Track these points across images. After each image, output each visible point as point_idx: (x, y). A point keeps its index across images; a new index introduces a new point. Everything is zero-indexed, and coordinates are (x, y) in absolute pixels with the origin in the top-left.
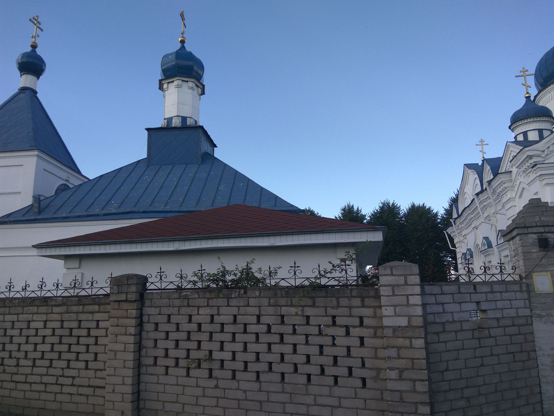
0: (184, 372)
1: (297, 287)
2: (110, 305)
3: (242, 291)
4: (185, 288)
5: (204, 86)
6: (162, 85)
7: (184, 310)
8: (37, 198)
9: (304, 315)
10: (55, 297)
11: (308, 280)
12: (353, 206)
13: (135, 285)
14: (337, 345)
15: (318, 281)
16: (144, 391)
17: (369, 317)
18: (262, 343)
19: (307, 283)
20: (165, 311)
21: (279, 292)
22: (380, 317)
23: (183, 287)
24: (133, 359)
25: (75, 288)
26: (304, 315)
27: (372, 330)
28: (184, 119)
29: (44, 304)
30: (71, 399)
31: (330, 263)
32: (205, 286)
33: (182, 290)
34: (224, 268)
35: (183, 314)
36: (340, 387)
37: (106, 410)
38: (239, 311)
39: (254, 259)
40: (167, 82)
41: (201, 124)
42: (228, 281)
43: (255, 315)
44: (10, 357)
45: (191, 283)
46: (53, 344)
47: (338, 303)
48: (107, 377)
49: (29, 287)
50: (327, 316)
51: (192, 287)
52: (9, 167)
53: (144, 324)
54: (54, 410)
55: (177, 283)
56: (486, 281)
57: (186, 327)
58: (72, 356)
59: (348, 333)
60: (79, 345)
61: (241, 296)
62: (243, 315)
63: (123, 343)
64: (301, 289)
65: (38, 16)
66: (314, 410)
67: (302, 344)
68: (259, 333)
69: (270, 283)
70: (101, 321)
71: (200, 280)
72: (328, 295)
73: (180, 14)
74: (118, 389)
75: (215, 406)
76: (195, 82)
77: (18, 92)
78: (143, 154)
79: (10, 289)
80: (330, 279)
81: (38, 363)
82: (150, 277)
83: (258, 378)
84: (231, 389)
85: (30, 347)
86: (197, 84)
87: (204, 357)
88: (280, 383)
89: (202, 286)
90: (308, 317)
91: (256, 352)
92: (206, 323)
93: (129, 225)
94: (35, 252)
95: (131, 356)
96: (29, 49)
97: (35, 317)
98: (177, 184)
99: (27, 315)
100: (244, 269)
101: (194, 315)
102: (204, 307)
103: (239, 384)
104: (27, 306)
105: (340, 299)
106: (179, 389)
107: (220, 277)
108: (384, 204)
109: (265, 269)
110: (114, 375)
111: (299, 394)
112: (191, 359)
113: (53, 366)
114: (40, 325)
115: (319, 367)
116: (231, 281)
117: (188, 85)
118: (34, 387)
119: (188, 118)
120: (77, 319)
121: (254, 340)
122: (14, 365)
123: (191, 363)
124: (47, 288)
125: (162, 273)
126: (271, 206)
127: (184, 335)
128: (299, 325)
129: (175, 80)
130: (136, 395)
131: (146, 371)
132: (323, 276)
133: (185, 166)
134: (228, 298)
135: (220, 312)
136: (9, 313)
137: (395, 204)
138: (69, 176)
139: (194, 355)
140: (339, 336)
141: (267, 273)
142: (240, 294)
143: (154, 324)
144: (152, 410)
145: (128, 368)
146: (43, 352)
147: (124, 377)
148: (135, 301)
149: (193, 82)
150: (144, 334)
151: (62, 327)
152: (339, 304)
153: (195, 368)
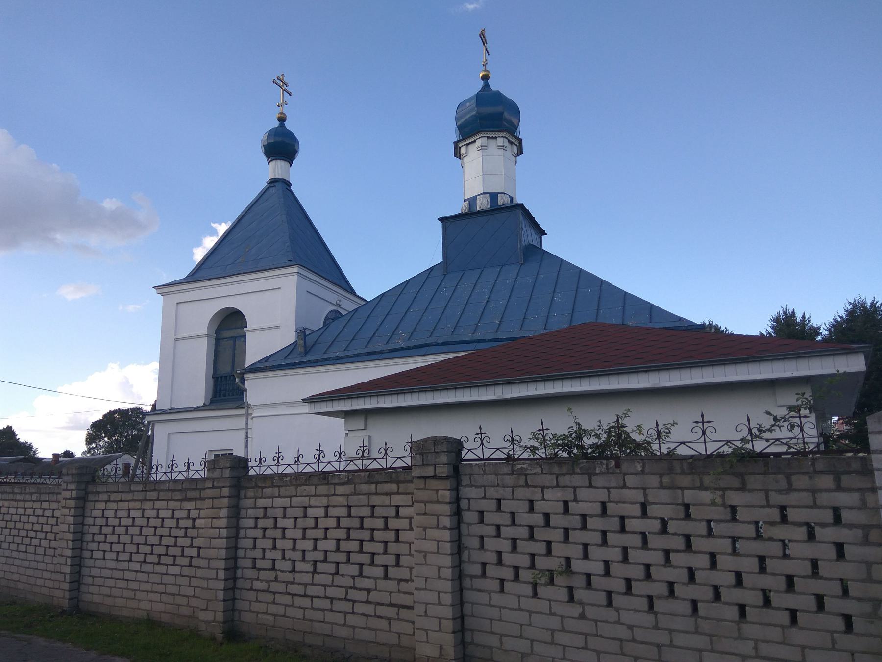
0: (528, 590)
1: (710, 457)
2: (413, 482)
3: (613, 463)
4: (520, 457)
5: (521, 141)
6: (459, 150)
7: (521, 493)
8: (302, 333)
9: (727, 504)
10: (337, 471)
11: (728, 444)
12: (793, 313)
13: (446, 453)
14: (791, 556)
15: (749, 446)
16: (470, 616)
17: (851, 508)
18: (655, 550)
19: (727, 450)
20: (492, 492)
21: (677, 466)
22: (873, 508)
23: (516, 456)
24: (451, 564)
25: (364, 459)
26: (727, 504)
27: (860, 532)
28: (493, 197)
29: (325, 482)
30: (367, 624)
31: (768, 413)
32: (550, 454)
33: (515, 461)
34: (579, 426)
35: (520, 499)
36: (802, 628)
37: (417, 643)
38: (609, 496)
39: (629, 411)
40: (466, 143)
41: (519, 200)
42: (587, 447)
43: (637, 503)
44: (284, 558)
45: (528, 450)
46: (338, 540)
47: (790, 483)
48: (416, 592)
49: (303, 458)
50: (768, 505)
51: (530, 457)
53: (463, 513)
54: (345, 639)
55: (507, 450)
56: (173, 479)
57: (525, 518)
58: (365, 558)
59: (811, 536)
60: (373, 543)
61: (611, 471)
62: (617, 502)
63: (435, 540)
64: (718, 460)
67: (725, 554)
68: (647, 533)
69: (660, 450)
70: (402, 506)
71: (541, 445)
72: (768, 469)
73: (480, 35)
74: (433, 610)
75: (582, 648)
76: (506, 136)
77: (267, 187)
78: (437, 257)
79: (278, 462)
80: (771, 442)
81: (320, 567)
82: (467, 441)
83: (651, 606)
84: (606, 622)
85: (308, 545)
86: (510, 139)
87: (559, 568)
88: (691, 616)
89: (546, 455)
90: (733, 509)
91: (644, 564)
92: (557, 514)
93: (427, 364)
94: (306, 408)
95: (447, 561)
97: (313, 501)
98: (489, 298)
99: (303, 498)
100: (613, 427)
101: (537, 501)
102: (552, 487)
103: (619, 614)
104: (301, 486)
105: (794, 478)
106: (523, 617)
107: (574, 441)
108: (854, 305)
109: (649, 426)
110: (426, 589)
111: (725, 637)
112: (538, 570)
113: (340, 573)
114: (320, 512)
115: (761, 593)
116: (591, 446)
118: (317, 603)
119: (499, 195)
120: (369, 504)
121: (640, 544)
122: (290, 570)
123: (540, 576)
124: (163, 470)
125: (482, 435)
126: (643, 322)
127: (523, 532)
128: (717, 521)
129: (499, 137)
130: (459, 621)
131: (472, 585)
132: (757, 436)
133: (499, 270)
134: (590, 474)
135: (578, 497)
136: (279, 495)
137: (876, 303)
138: (340, 298)
139: (542, 563)
140: (796, 541)
141: (654, 433)
142: (609, 467)
143: (477, 513)
144: (484, 647)
145: (445, 579)
146: (326, 552)
147: (439, 592)
148: (447, 477)
149: (505, 137)
150: (463, 527)
151: (349, 516)
152: (792, 485)
153: (546, 585)
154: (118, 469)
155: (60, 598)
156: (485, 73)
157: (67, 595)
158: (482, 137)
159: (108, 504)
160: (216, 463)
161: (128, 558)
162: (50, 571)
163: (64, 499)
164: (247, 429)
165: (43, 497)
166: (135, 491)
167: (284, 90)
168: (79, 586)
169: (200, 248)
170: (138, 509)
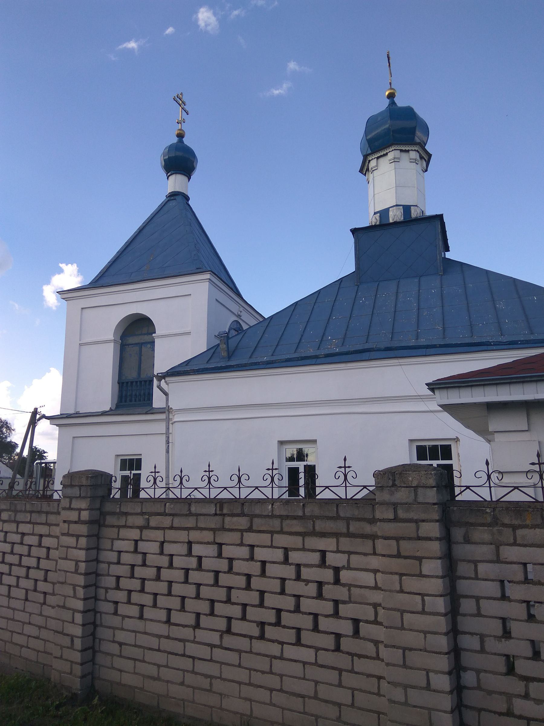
28: (407, 209)
40: (377, 156)
52: (172, 298)
65: (182, 93)
66: (350, 716)
76: (419, 150)
77: (167, 200)
86: (421, 153)
96: (175, 140)
117: (409, 156)
119: (412, 207)
154: (159, 479)
155: (64, 673)
156: (392, 91)
157: (78, 670)
158: (395, 150)
159: (145, 532)
160: (397, 476)
161: (192, 622)
162: (36, 626)
163: (65, 522)
164: (168, 434)
165: (20, 517)
166: (201, 515)
168: (94, 656)
169: (49, 286)
170: (208, 543)
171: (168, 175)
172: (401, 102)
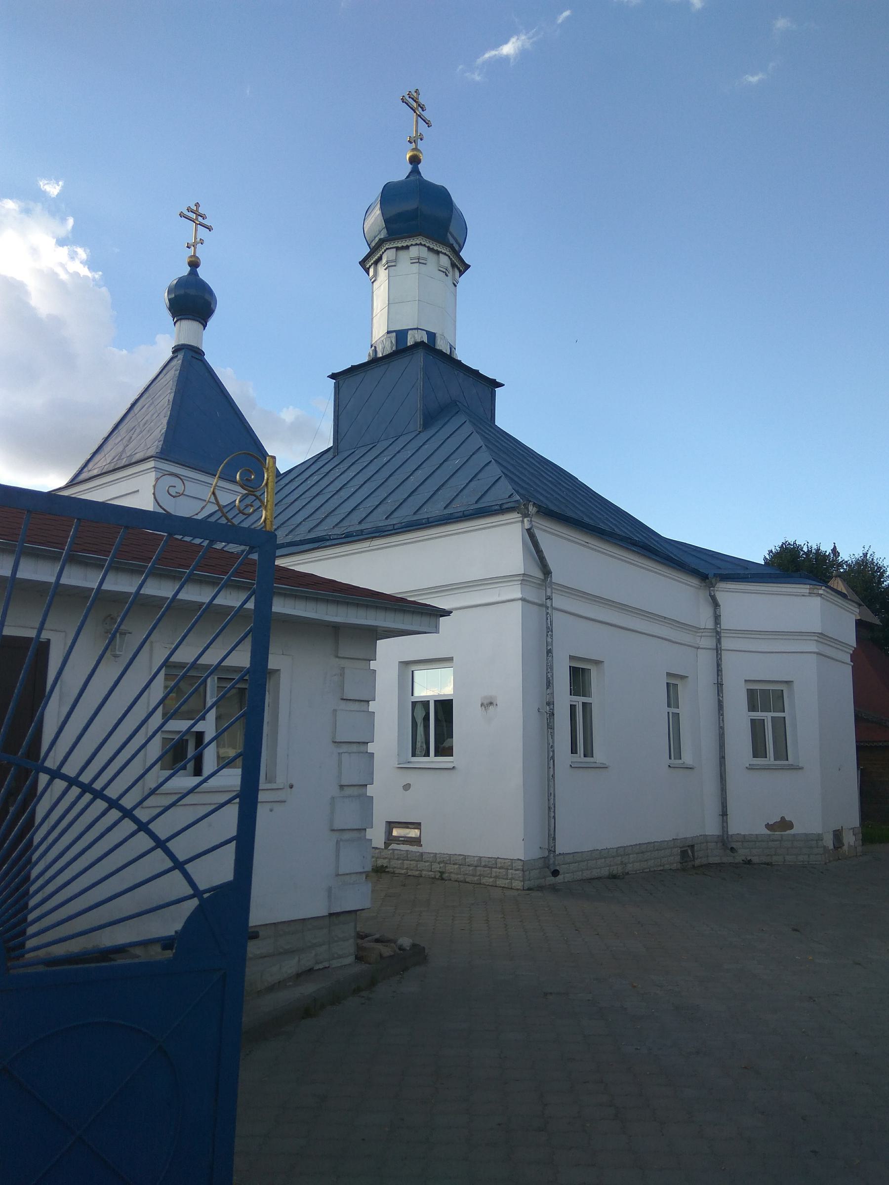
29: (366, 944)
40: (372, 262)
76: (423, 243)
86: (431, 246)
129: (412, 245)
158: (387, 249)
167: (419, 116)
171: (175, 321)
172: (429, 173)
